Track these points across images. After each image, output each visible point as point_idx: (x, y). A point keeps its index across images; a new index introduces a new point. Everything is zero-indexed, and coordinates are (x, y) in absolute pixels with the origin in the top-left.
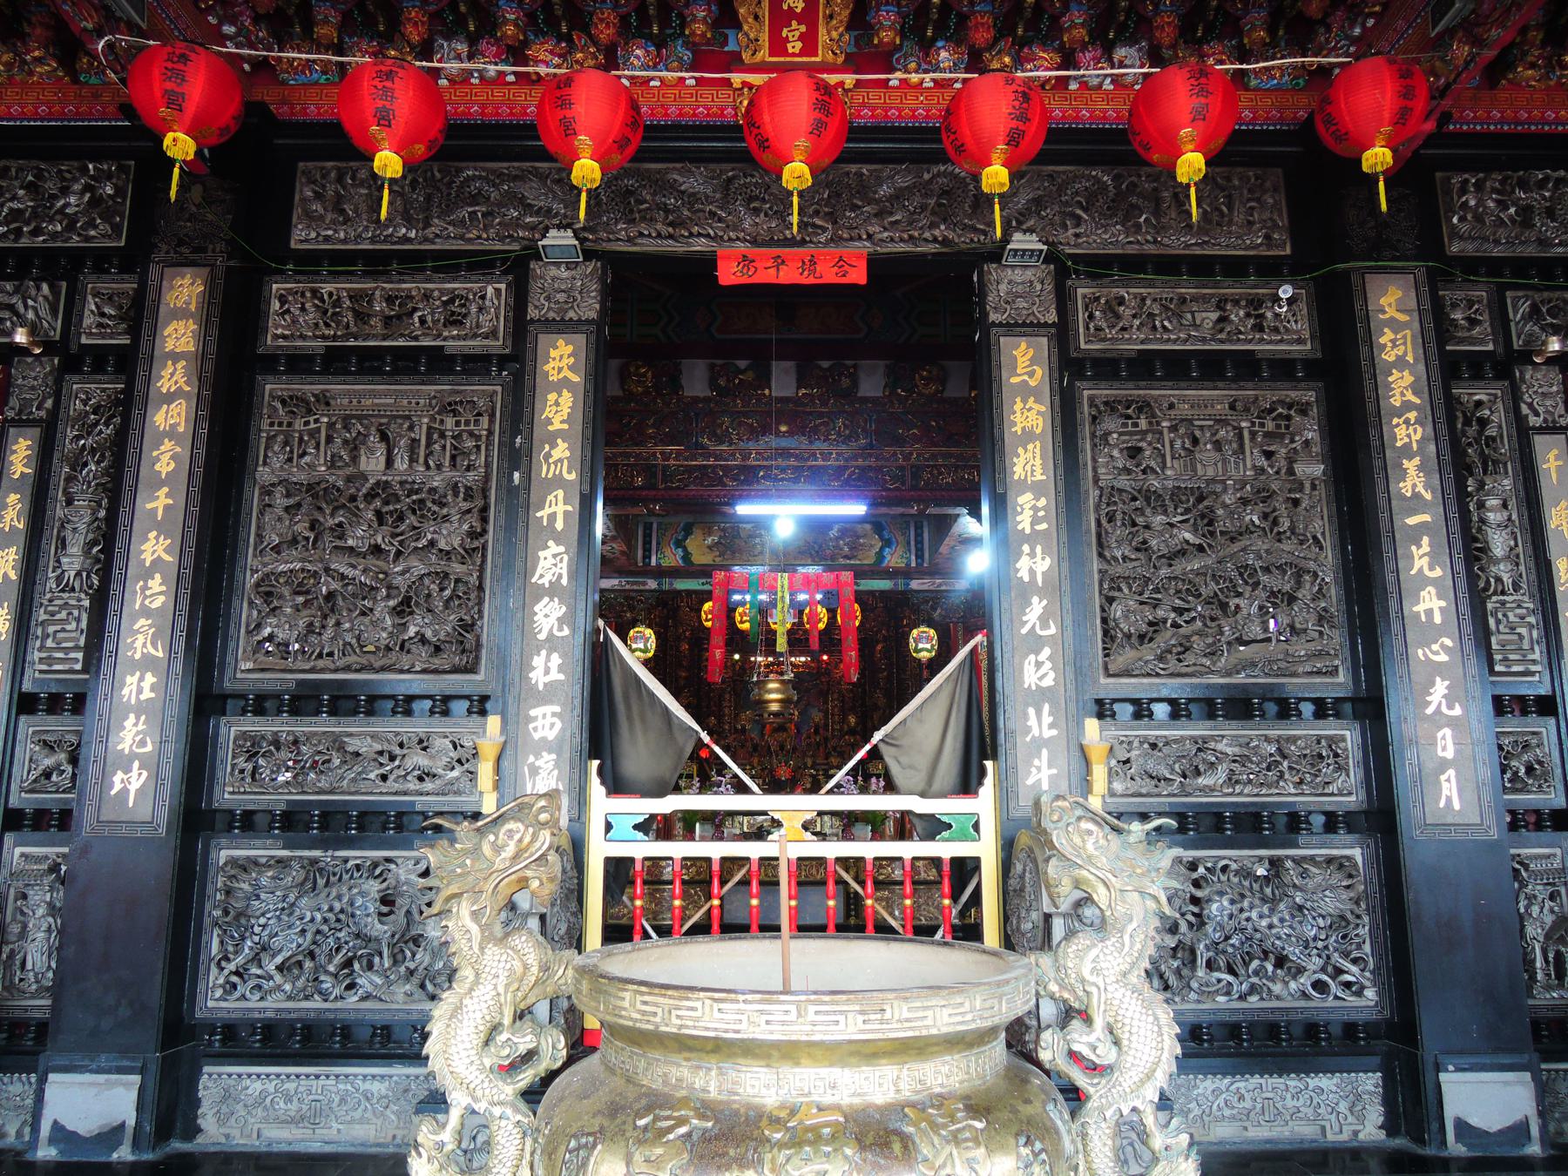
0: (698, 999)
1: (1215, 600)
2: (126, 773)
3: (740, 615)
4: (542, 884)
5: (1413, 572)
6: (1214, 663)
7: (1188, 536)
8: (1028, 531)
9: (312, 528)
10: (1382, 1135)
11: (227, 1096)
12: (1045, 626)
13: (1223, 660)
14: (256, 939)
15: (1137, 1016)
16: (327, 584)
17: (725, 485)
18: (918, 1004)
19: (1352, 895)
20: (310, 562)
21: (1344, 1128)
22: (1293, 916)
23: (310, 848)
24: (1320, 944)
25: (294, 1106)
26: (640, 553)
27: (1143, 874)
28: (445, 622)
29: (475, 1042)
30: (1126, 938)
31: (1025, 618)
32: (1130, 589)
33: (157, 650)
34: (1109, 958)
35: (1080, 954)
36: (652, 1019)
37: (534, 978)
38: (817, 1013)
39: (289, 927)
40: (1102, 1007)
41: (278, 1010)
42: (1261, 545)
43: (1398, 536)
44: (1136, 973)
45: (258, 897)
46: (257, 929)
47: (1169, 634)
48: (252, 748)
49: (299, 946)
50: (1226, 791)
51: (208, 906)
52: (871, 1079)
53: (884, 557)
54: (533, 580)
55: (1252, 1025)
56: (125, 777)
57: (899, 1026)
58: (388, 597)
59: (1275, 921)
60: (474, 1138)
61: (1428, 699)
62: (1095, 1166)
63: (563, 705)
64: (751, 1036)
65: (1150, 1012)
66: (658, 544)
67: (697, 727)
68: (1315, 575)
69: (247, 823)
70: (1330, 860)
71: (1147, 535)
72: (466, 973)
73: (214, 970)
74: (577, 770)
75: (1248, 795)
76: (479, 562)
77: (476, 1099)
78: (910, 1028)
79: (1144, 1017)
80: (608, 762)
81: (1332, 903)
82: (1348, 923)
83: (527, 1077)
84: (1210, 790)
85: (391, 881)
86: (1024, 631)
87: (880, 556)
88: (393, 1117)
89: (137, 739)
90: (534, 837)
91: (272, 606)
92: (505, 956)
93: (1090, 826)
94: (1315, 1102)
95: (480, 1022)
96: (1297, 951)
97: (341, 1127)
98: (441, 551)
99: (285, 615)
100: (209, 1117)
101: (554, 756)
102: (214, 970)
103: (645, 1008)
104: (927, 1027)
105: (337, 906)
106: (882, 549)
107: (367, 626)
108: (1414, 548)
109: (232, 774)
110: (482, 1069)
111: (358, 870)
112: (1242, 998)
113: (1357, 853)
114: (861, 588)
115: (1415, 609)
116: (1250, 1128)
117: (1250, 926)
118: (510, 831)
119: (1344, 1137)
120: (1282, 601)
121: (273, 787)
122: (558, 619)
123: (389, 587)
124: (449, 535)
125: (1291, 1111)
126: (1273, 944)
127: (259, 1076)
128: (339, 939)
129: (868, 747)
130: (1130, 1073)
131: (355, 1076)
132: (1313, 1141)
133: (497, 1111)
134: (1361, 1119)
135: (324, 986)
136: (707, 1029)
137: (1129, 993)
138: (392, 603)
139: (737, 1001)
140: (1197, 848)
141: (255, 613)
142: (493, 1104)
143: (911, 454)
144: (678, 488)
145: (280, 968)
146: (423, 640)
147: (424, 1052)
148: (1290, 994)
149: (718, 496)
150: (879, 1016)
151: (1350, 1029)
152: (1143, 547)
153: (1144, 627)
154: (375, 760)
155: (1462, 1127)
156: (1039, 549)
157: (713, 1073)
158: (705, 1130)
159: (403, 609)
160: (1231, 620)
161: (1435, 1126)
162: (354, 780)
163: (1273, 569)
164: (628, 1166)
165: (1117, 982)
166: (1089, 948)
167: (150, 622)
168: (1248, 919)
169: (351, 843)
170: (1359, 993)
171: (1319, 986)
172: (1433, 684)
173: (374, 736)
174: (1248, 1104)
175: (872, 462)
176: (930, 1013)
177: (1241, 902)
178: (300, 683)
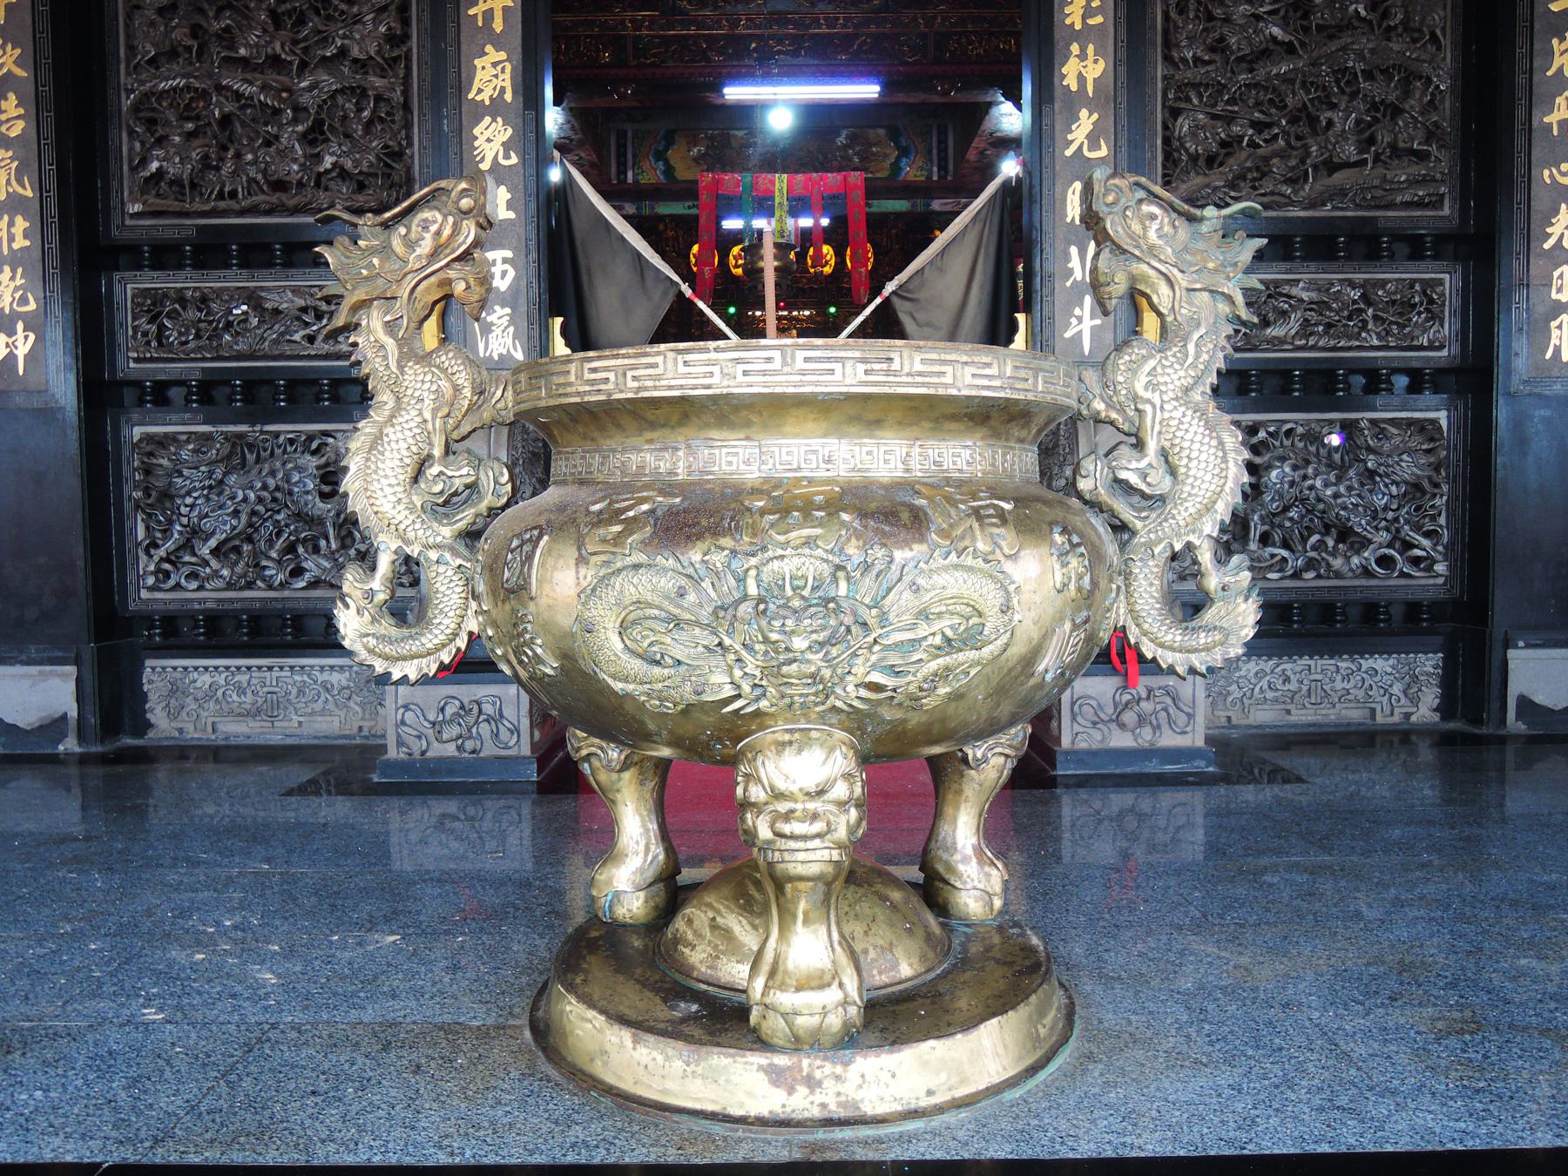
0: (658, 354)
1: (1303, 115)
2: (10, 336)
3: (735, 257)
4: (468, 287)
5: (1549, 73)
6: (1295, 192)
7: (1276, 31)
8: (1078, 26)
9: (194, 36)
10: (1436, 717)
11: (174, 690)
12: (1094, 146)
13: (1307, 188)
14: (185, 520)
15: (1199, 437)
16: (218, 104)
17: (709, 60)
18: (934, 356)
19: (1432, 460)
20: (195, 77)
21: (1397, 711)
22: (1362, 484)
23: (234, 423)
24: (1390, 515)
25: (249, 698)
26: (613, 170)
27: (1216, 270)
28: (367, 150)
29: (402, 477)
30: (1191, 347)
31: (1070, 137)
32: (1201, 101)
33: (24, 187)
34: (1168, 370)
35: (1133, 370)
36: (602, 387)
37: (466, 403)
38: (807, 360)
39: (220, 508)
40: (1157, 428)
41: (219, 600)
42: (1365, 43)
43: (1537, 27)
44: (1201, 389)
45: (181, 475)
46: (184, 510)
47: (1244, 155)
48: (152, 307)
49: (234, 528)
50: (1298, 343)
51: (126, 489)
52: (875, 454)
53: (900, 169)
54: (470, 96)
55: (1304, 606)
56: (10, 341)
57: (910, 379)
58: (295, 121)
59: (1342, 489)
60: (442, 710)
61: (1549, 230)
62: (1138, 608)
63: (514, 250)
64: (725, 391)
65: (1214, 434)
66: (634, 156)
67: (676, 278)
68: (1429, 81)
69: (159, 395)
70: (1410, 423)
71: (1225, 30)
72: (385, 398)
73: (143, 557)
74: (536, 327)
75: (1324, 349)
76: (401, 73)
77: (408, 542)
78: (923, 385)
79: (1207, 439)
80: (574, 322)
81: (1408, 468)
82: (1424, 492)
83: (465, 518)
84: (1276, 343)
85: (330, 455)
86: (1068, 153)
87: (896, 168)
88: (358, 709)
89: (17, 296)
90: (456, 229)
91: (157, 135)
92: (429, 377)
93: (1155, 209)
94: (1367, 685)
95: (406, 453)
96: (1363, 522)
97: (301, 719)
98: (355, 61)
99: (174, 146)
100: (158, 710)
101: (508, 310)
102: (143, 557)
103: (593, 376)
104: (945, 386)
105: (271, 482)
106: (898, 159)
107: (271, 157)
108: (1555, 42)
109: (134, 337)
110: (411, 508)
111: (292, 445)
112: (1296, 575)
113: (1442, 417)
114: (873, 210)
115: (1546, 120)
116: (1293, 712)
117: (1313, 495)
118: (425, 220)
119: (1396, 718)
120: (1384, 116)
121: (183, 352)
122: (503, 144)
123: (297, 109)
124: (363, 38)
125: (1340, 694)
126: (1337, 514)
127: (206, 668)
128: (278, 521)
129: (878, 300)
130: (1186, 504)
131: (312, 667)
132: (1360, 724)
133: (433, 555)
134: (1415, 701)
135: (268, 573)
136: (670, 388)
137: (1189, 413)
138: (300, 128)
139: (707, 350)
140: (1258, 412)
141: (138, 145)
142: (428, 547)
143: (935, 18)
144: (653, 65)
145: (215, 552)
146: (344, 174)
147: (341, 490)
148: (1351, 570)
149: (701, 75)
150: (884, 366)
151: (1413, 610)
152: (1219, 47)
153: (1214, 147)
154: (298, 319)
155: (1525, 704)
156: (1091, 49)
157: (681, 453)
158: (671, 506)
159: (314, 137)
160: (1321, 138)
161: (1495, 705)
162: (276, 342)
163: (1377, 74)
164: (579, 549)
165: (1177, 399)
166: (1145, 359)
167: (10, 153)
168: (1311, 488)
169: (282, 417)
170: (1429, 569)
171: (1385, 561)
172: (1557, 212)
173: (296, 291)
174: (1293, 686)
175: (887, 28)
176: (948, 369)
177: (1306, 468)
178: (200, 228)
